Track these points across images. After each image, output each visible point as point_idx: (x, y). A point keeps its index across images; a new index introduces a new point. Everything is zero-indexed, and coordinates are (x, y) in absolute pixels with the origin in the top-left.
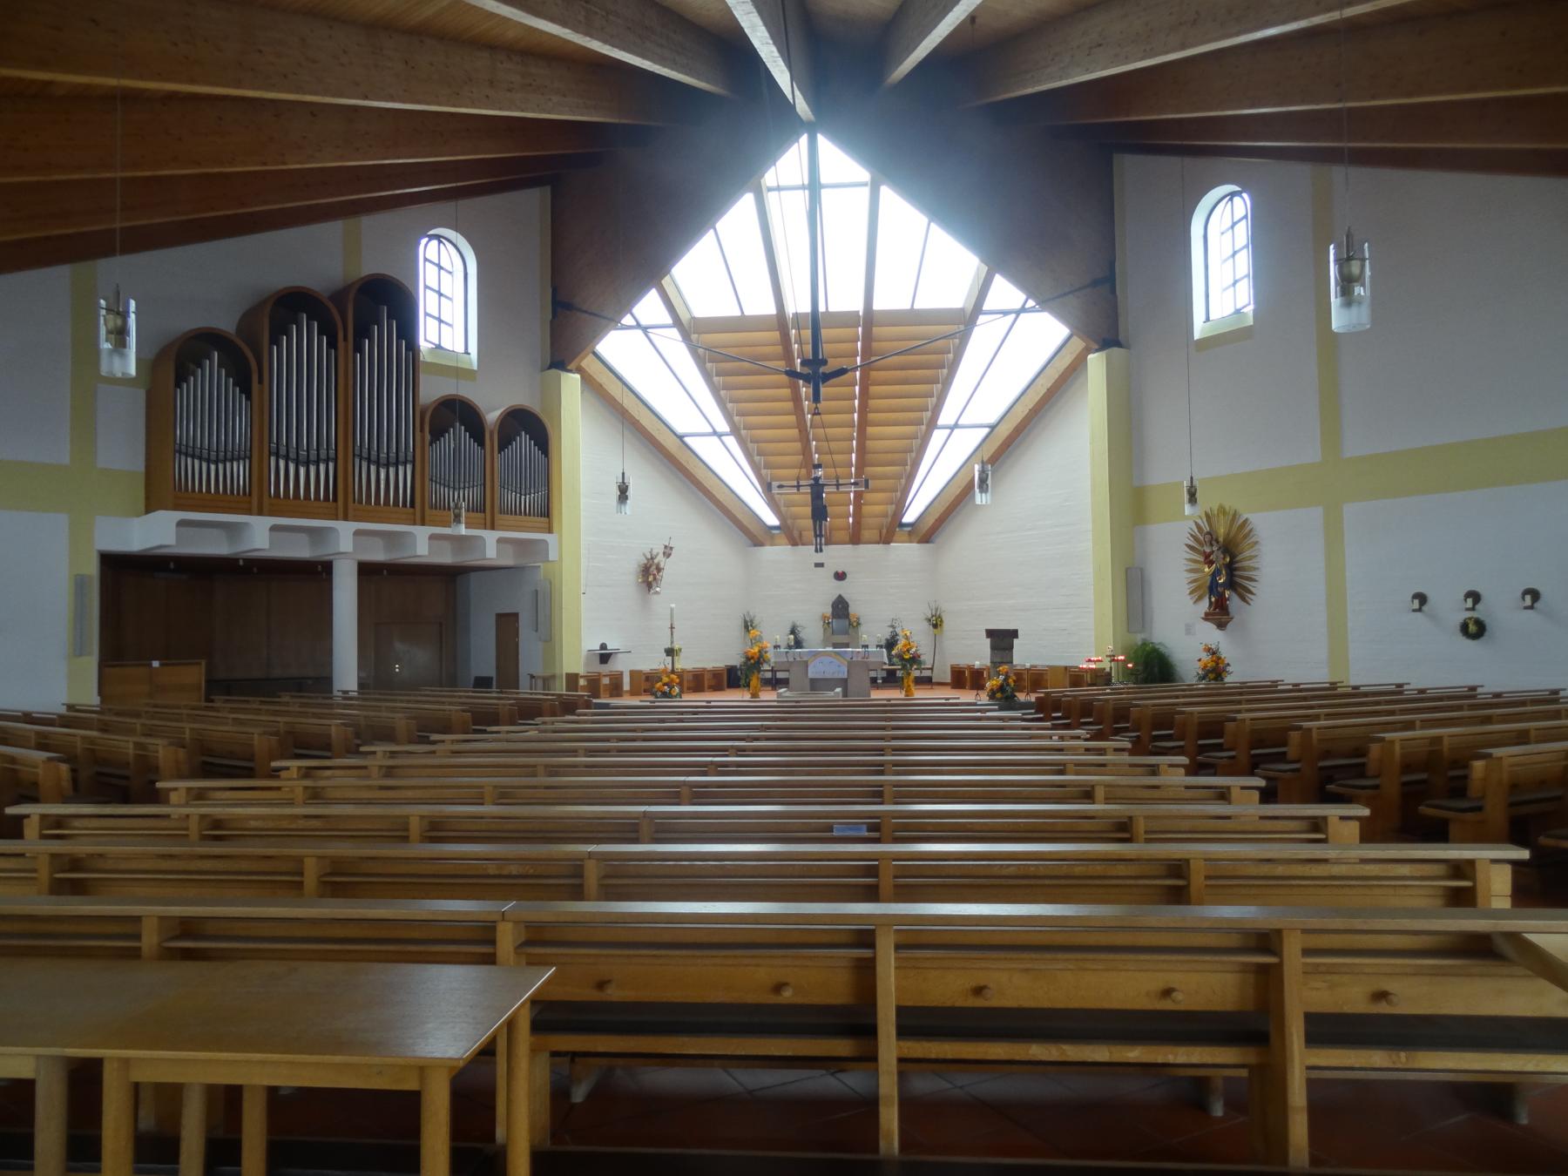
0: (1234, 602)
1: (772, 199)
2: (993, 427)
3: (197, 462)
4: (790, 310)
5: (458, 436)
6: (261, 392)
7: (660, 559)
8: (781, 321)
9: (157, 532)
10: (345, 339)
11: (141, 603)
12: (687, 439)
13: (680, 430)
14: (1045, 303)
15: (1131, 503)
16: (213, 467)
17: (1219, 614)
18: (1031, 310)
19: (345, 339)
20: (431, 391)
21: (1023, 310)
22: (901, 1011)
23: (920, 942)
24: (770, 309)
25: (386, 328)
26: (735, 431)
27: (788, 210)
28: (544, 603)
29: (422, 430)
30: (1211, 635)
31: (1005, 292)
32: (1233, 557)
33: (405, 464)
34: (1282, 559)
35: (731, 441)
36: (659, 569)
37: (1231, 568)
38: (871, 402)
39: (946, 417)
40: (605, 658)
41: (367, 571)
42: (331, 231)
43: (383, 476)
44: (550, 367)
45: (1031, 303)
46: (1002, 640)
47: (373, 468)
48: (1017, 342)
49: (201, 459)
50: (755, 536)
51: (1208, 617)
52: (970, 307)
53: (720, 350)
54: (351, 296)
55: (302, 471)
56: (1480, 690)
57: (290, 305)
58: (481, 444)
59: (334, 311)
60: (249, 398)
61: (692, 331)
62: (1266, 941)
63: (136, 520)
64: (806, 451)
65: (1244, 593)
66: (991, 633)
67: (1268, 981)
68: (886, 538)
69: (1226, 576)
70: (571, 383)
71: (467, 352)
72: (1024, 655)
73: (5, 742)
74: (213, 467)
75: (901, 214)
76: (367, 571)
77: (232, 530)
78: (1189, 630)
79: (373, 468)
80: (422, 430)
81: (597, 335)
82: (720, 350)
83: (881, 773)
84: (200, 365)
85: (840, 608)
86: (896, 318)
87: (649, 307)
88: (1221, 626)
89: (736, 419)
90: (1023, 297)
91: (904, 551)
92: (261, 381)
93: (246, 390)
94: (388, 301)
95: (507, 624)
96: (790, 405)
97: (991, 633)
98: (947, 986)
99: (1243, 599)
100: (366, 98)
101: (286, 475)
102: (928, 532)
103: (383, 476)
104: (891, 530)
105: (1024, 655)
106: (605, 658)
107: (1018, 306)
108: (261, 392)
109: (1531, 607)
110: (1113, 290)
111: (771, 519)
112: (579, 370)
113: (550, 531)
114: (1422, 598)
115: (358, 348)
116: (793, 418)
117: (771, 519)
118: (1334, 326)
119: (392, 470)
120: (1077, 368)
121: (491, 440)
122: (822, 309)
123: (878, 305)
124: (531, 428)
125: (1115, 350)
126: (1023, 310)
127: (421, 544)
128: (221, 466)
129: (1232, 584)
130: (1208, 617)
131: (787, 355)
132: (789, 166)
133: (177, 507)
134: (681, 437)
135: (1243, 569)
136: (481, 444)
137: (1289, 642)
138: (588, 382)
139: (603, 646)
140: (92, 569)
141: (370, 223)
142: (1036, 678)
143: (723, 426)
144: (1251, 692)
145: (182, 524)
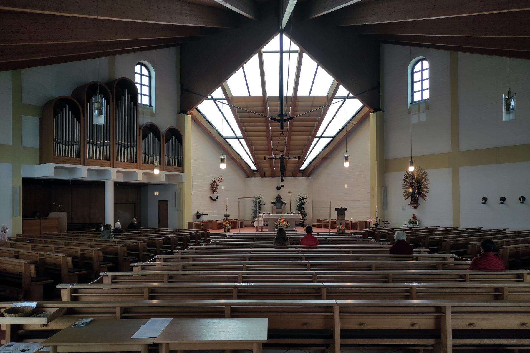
0: (420, 199)
1: (264, 55)
2: (334, 138)
3: (61, 145)
4: (269, 93)
5: (152, 136)
6: (84, 120)
7: (217, 181)
8: (264, 98)
9: (47, 171)
10: (113, 101)
11: (37, 197)
12: (227, 140)
13: (225, 135)
14: (356, 96)
15: (385, 164)
16: (67, 147)
17: (415, 203)
18: (351, 98)
19: (113, 101)
20: (144, 120)
21: (347, 97)
22: (342, 331)
23: (344, 311)
24: (260, 94)
25: (127, 98)
26: (244, 137)
27: (271, 61)
28: (178, 198)
29: (139, 135)
30: (411, 212)
31: (342, 91)
32: (420, 184)
33: (134, 147)
34: (438, 184)
35: (243, 141)
36: (217, 185)
37: (419, 188)
38: (294, 128)
39: (319, 134)
40: (198, 216)
41: (117, 185)
42: (104, 61)
43: (126, 151)
44: (181, 112)
45: (351, 95)
46: (341, 211)
47: (123, 148)
48: (346, 108)
49: (63, 144)
50: (248, 173)
51: (411, 204)
52: (330, 96)
53: (243, 109)
54: (115, 85)
55: (98, 149)
56: (507, 230)
57: (92, 90)
58: (160, 140)
59: (109, 91)
60: (79, 122)
61: (230, 99)
62: (439, 310)
63: (36, 167)
64: (269, 145)
65: (424, 197)
66: (337, 209)
67: (440, 321)
68: (294, 175)
69: (417, 190)
70: (188, 118)
71: (150, 105)
72: (349, 217)
73: (1, 246)
74: (67, 147)
75: (309, 63)
76: (117, 185)
77: (70, 170)
78: (404, 208)
79: (123, 148)
80: (139, 135)
81: (199, 102)
82: (243, 109)
83: (251, 257)
84: (62, 110)
85: (279, 199)
86: (304, 98)
87: (218, 93)
88: (415, 207)
89: (245, 132)
90: (348, 92)
91: (301, 180)
92: (84, 116)
93: (79, 119)
94: (128, 88)
95: (163, 205)
96: (264, 128)
97: (337, 209)
98: (353, 324)
99: (423, 198)
100: (146, 20)
101: (93, 151)
102: (308, 173)
103: (126, 151)
104: (297, 173)
105: (349, 217)
106: (198, 216)
107: (346, 95)
108: (84, 120)
109: (522, 203)
110: (379, 92)
111: (254, 168)
112: (191, 114)
113: (182, 171)
114: (485, 199)
115: (117, 105)
116: (265, 133)
117: (254, 168)
118: (504, 120)
119: (129, 149)
120: (366, 117)
121: (163, 140)
122: (285, 94)
123: (299, 94)
124: (176, 135)
125: (379, 112)
126: (347, 97)
127: (139, 176)
128: (70, 147)
129: (419, 193)
130: (411, 204)
131: (265, 111)
132: (273, 44)
133: (54, 162)
134: (224, 139)
135: (422, 188)
136: (159, 139)
137: (437, 213)
138: (195, 120)
139: (198, 212)
140: (20, 184)
141: (119, 58)
142: (354, 225)
143: (240, 134)
144: (427, 230)
145: (56, 168)
